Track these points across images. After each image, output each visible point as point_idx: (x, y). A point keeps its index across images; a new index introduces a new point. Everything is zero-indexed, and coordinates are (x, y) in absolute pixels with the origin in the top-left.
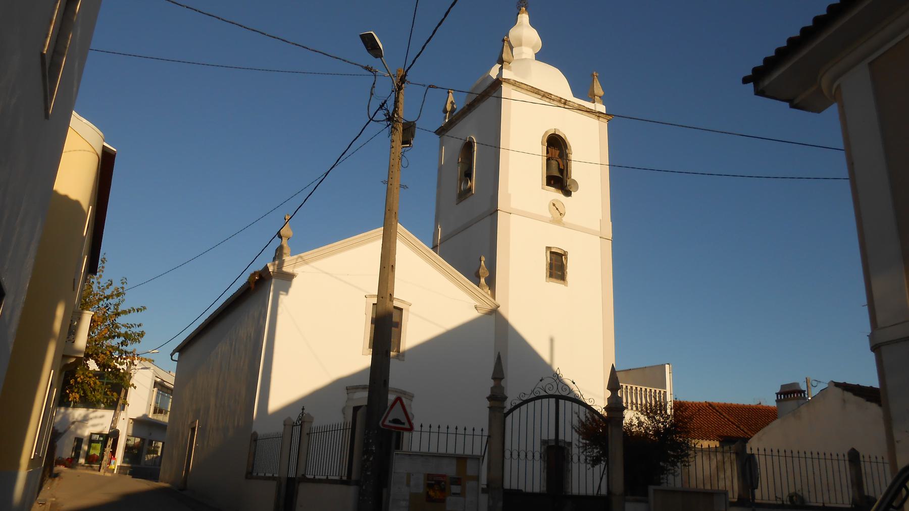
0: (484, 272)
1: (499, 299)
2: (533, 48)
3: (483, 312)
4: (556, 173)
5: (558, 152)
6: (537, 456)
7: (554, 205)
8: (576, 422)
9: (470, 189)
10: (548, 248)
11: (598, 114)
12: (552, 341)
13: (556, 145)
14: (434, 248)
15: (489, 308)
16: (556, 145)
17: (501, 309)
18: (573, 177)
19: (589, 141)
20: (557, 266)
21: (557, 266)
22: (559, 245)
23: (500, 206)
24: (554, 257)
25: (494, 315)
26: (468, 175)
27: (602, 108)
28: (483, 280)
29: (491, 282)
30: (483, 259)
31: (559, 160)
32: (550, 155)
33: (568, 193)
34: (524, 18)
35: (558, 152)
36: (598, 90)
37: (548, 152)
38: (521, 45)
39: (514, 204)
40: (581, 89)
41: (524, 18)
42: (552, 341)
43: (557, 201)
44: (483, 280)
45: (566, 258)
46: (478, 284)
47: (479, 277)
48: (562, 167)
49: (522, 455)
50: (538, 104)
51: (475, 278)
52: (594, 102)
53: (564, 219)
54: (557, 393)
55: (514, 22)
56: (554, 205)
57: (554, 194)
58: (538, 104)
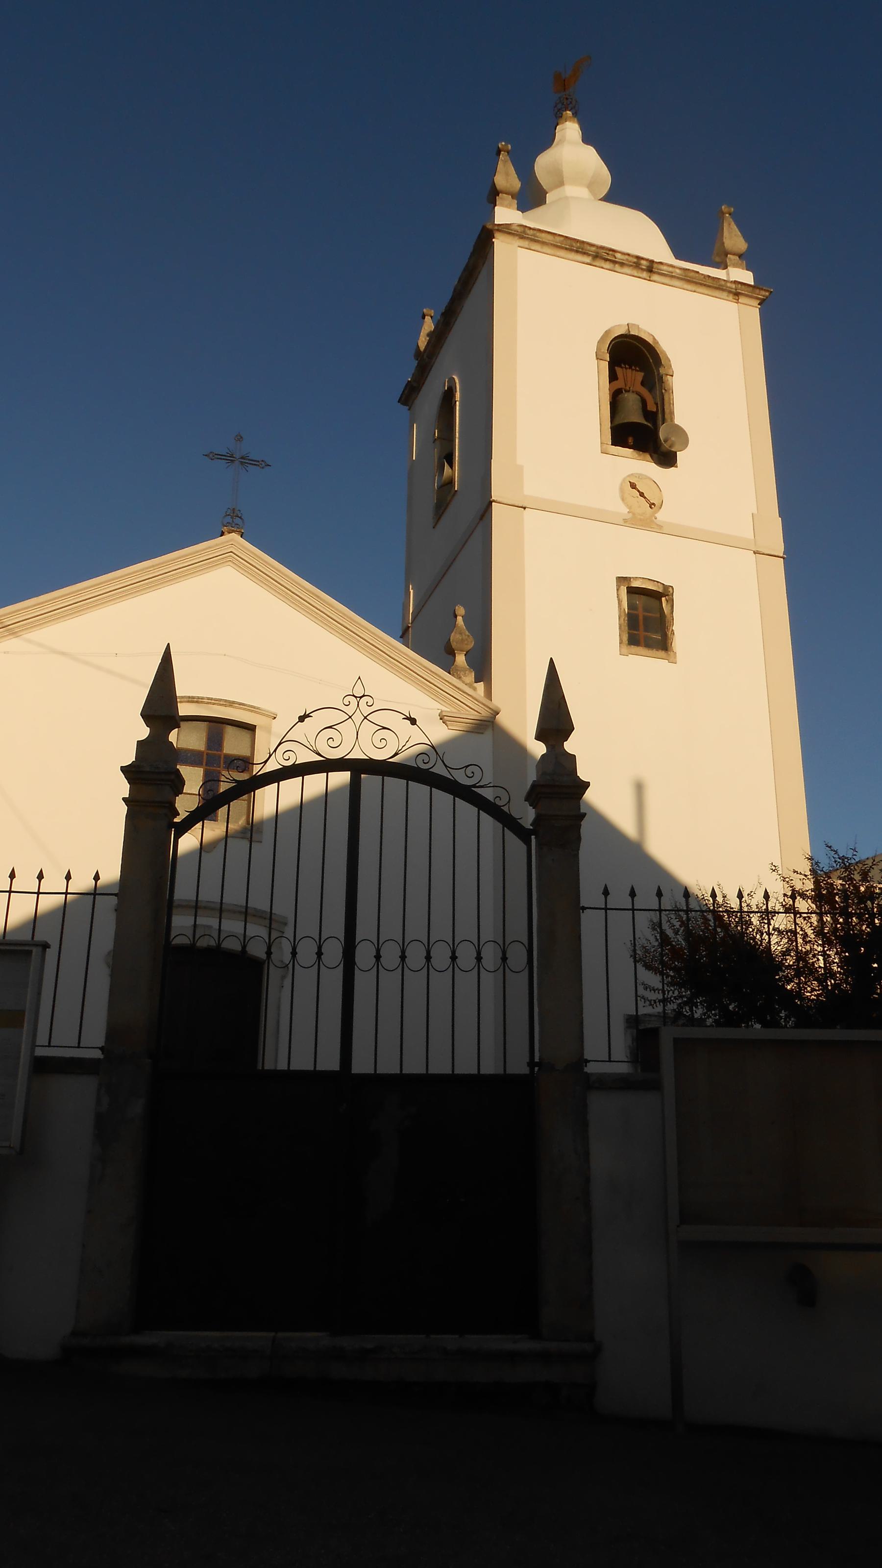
0: (461, 634)
1: (498, 700)
2: (591, 186)
3: (462, 727)
4: (636, 417)
5: (640, 376)
6: (518, 956)
7: (633, 486)
8: (647, 936)
9: (451, 482)
10: (621, 580)
11: (736, 291)
12: (639, 788)
13: (633, 361)
14: (403, 636)
15: (474, 715)
16: (633, 361)
17: (502, 719)
18: (678, 421)
19: (715, 349)
20: (647, 619)
21: (647, 619)
22: (648, 571)
23: (496, 493)
24: (640, 601)
25: (488, 734)
26: (449, 458)
27: (747, 277)
28: (461, 659)
29: (481, 668)
30: (461, 610)
31: (644, 392)
32: (619, 384)
33: (667, 459)
34: (570, 131)
35: (640, 376)
36: (733, 238)
37: (613, 377)
38: (561, 183)
39: (533, 487)
40: (693, 241)
41: (570, 131)
42: (639, 788)
43: (640, 476)
44: (461, 659)
45: (671, 602)
46: (448, 666)
47: (451, 652)
48: (651, 407)
49: (416, 956)
50: (575, 274)
51: (443, 656)
52: (726, 267)
53: (661, 516)
54: (357, 755)
55: (547, 140)
56: (633, 486)
57: (633, 464)
58: (575, 274)
